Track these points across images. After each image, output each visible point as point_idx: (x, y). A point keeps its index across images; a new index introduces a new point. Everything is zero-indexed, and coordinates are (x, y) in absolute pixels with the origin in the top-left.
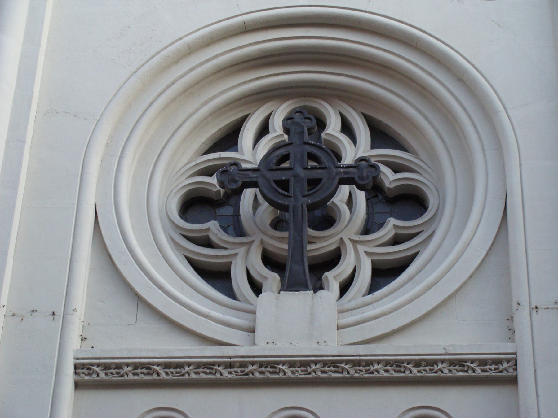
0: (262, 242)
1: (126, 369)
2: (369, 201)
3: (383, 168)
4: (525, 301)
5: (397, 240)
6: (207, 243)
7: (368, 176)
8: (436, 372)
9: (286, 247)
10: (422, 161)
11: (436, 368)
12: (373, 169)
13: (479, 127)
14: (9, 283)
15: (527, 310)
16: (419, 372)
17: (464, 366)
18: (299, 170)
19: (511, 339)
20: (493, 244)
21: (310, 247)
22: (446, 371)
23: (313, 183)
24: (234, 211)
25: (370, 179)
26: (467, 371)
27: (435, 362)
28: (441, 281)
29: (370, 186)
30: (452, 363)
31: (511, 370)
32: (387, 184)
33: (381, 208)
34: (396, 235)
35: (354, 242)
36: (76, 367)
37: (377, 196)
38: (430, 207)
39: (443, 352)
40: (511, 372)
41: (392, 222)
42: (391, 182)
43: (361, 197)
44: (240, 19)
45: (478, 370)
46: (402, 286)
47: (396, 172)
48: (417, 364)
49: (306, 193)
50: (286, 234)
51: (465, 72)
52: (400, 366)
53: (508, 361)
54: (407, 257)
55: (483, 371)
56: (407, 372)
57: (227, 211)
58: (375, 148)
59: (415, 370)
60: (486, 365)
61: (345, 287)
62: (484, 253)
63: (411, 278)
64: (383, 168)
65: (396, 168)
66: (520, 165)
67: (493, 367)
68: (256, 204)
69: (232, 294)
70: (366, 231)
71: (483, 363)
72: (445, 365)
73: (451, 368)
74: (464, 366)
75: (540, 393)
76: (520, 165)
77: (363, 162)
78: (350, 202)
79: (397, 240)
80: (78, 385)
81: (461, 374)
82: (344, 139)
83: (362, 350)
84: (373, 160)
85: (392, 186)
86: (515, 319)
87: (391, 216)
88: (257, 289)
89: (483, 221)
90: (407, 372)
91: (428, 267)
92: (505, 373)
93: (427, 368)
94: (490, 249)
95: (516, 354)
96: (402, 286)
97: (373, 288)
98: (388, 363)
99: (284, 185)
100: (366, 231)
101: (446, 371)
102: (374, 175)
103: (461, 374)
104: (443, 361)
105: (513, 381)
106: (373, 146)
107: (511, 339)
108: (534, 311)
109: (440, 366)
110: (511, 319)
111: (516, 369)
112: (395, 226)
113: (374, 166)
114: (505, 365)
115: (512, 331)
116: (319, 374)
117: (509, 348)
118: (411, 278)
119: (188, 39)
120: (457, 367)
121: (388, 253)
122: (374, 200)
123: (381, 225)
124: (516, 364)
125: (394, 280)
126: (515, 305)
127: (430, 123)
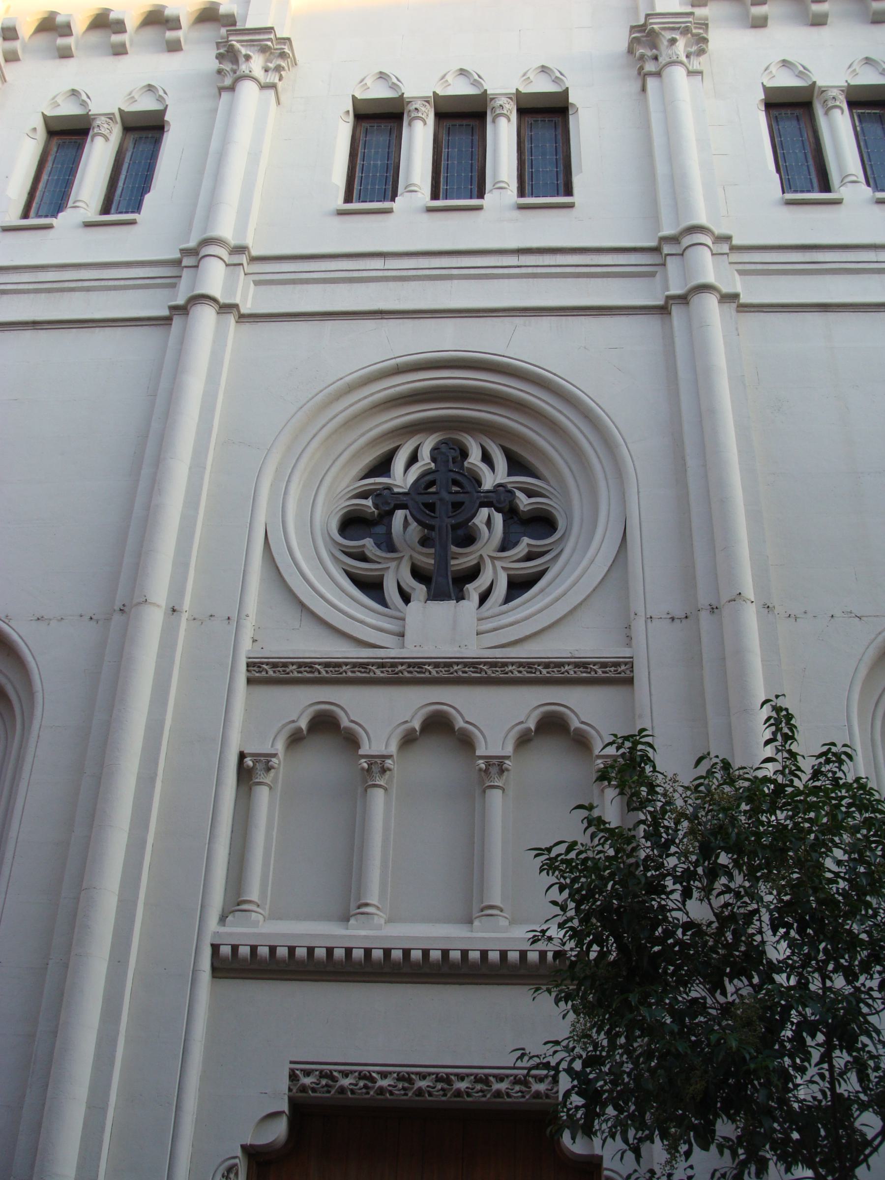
0: (411, 557)
1: (291, 668)
3: (519, 494)
4: (641, 612)
5: (529, 557)
6: (362, 557)
8: (563, 673)
9: (432, 562)
10: (550, 486)
11: (563, 670)
12: (510, 494)
15: (644, 619)
16: (548, 673)
17: (587, 668)
18: (444, 495)
19: (629, 645)
20: (614, 561)
21: (453, 562)
22: (572, 672)
23: (457, 506)
26: (590, 673)
27: (562, 665)
30: (577, 665)
31: (628, 672)
32: (522, 508)
34: (529, 553)
35: (492, 558)
36: (248, 665)
37: (512, 518)
38: (559, 528)
39: (569, 655)
41: (526, 540)
43: (498, 518)
44: (393, 362)
47: (529, 497)
48: (547, 666)
49: (451, 514)
50: (432, 551)
51: (591, 410)
53: (626, 664)
55: (604, 672)
56: (538, 673)
57: (380, 529)
59: (544, 671)
61: (484, 597)
62: (606, 569)
63: (542, 591)
64: (519, 494)
65: (530, 494)
66: (638, 492)
67: (612, 669)
68: (406, 524)
69: (383, 602)
70: (503, 548)
71: (604, 665)
72: (570, 667)
73: (576, 669)
74: (587, 668)
77: (501, 488)
78: (489, 523)
79: (529, 557)
80: (250, 681)
81: (584, 675)
82: (484, 467)
83: (498, 653)
84: (509, 486)
86: (632, 627)
87: (525, 536)
88: (406, 598)
90: (538, 673)
92: (623, 675)
93: (555, 670)
95: (632, 658)
97: (508, 599)
98: (521, 665)
99: (431, 507)
100: (503, 548)
101: (572, 672)
103: (584, 675)
104: (569, 664)
106: (510, 474)
107: (629, 645)
108: (649, 620)
109: (567, 668)
111: (632, 671)
112: (528, 545)
113: (511, 492)
114: (623, 667)
115: (629, 637)
116: (460, 673)
117: (626, 652)
118: (542, 591)
119: (348, 379)
125: (526, 592)
126: (632, 615)
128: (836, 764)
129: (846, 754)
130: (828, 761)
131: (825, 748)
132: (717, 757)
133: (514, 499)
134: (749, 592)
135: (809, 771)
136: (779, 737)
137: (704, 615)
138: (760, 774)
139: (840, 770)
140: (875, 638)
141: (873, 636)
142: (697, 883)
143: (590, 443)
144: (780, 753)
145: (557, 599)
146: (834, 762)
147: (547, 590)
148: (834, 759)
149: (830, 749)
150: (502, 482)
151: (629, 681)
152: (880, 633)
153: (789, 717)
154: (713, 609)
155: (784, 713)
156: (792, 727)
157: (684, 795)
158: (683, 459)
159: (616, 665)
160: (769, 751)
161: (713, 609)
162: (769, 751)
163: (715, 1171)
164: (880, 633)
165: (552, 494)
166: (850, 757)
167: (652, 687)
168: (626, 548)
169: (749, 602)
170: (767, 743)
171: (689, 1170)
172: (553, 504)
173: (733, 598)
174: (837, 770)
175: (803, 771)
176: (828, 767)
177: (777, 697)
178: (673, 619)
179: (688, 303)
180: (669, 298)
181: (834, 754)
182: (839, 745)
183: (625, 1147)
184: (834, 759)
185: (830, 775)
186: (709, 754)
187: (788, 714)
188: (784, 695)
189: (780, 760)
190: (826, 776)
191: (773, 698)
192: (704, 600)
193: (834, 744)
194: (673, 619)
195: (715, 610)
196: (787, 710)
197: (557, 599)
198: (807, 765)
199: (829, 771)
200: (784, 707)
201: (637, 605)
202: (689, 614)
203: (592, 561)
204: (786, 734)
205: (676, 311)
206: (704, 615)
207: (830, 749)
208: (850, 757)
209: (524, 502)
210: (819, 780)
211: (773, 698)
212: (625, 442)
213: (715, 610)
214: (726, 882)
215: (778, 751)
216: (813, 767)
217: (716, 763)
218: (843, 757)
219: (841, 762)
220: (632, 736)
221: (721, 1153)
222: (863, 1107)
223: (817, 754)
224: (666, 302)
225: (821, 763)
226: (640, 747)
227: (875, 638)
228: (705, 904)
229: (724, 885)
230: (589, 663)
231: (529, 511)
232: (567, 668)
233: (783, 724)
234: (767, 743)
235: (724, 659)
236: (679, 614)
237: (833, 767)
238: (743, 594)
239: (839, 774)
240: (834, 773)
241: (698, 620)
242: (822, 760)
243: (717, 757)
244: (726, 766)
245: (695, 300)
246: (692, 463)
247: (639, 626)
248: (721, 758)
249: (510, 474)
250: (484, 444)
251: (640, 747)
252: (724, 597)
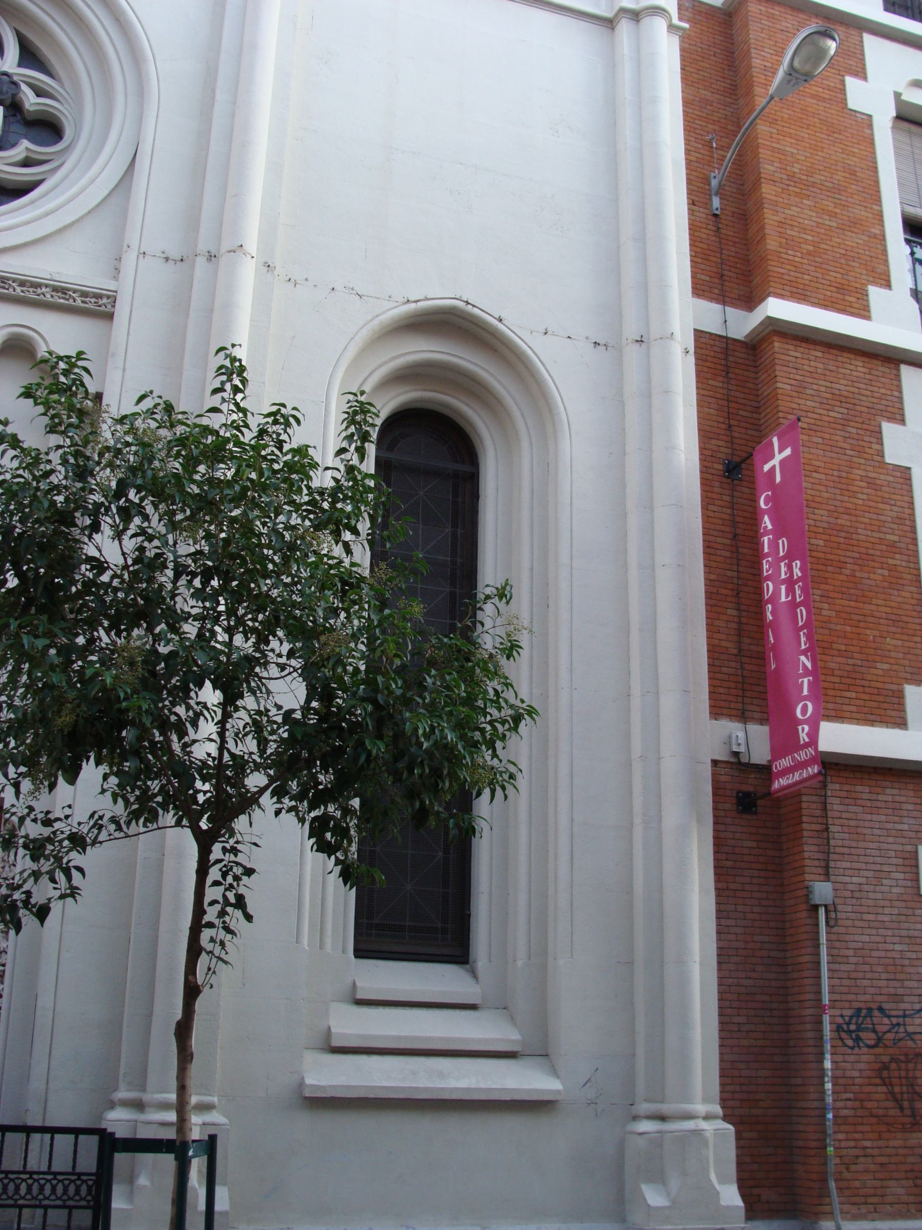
2: (725, 340)
3: (24, 87)
4: (135, 244)
5: (27, 163)
7: (7, 92)
8: (38, 295)
10: (64, 89)
11: (39, 291)
12: (13, 86)
13: (126, 72)
14: (256, 240)
15: (136, 253)
16: (22, 291)
17: (66, 294)
19: (116, 278)
20: (116, 186)
22: (48, 296)
24: (735, 340)
25: (10, 95)
26: (68, 300)
27: (39, 285)
28: (61, 210)
29: (8, 102)
30: (55, 289)
31: (109, 306)
32: (27, 106)
33: (17, 128)
34: (27, 158)
37: (15, 115)
38: (65, 137)
39: (49, 277)
40: (109, 308)
41: (25, 144)
42: (31, 104)
45: (79, 300)
46: (25, 206)
47: (38, 96)
48: (22, 284)
51: (123, 12)
52: (5, 283)
53: (108, 297)
54: (31, 181)
55: (83, 302)
56: (11, 290)
58: (695, 335)
59: (18, 289)
60: (87, 297)
62: (106, 192)
63: (32, 202)
64: (24, 87)
65: (39, 93)
66: (157, 116)
67: (93, 300)
71: (84, 294)
72: (48, 290)
73: (54, 293)
74: (66, 294)
75: (131, 332)
76: (157, 116)
77: (5, 77)
79: (27, 163)
81: (62, 301)
84: (15, 78)
85: (32, 109)
86: (123, 260)
87: (26, 138)
89: (111, 161)
90: (11, 290)
91: (50, 195)
92: (103, 308)
93: (31, 290)
94: (113, 190)
95: (116, 292)
96: (25, 206)
101: (48, 296)
102: (14, 92)
103: (62, 301)
104: (47, 286)
105: (110, 316)
106: (20, 65)
107: (116, 278)
108: (142, 256)
109: (44, 290)
110: (119, 259)
111: (114, 306)
112: (27, 149)
113: (15, 84)
114: (105, 301)
115: (117, 270)
117: (111, 285)
118: (32, 202)
120: (60, 294)
121: (16, 174)
122: (12, 119)
123: (14, 145)
124: (115, 302)
125: (12, 201)
126: (125, 247)
127: (80, 55)
128: (283, 427)
129: (294, 417)
130: (276, 422)
131: (275, 409)
132: (160, 397)
133: (18, 93)
134: (252, 245)
135: (255, 429)
136: (228, 387)
137: (201, 261)
138: (205, 421)
139: (285, 432)
140: (372, 320)
141: (370, 317)
142: (108, 520)
143: (116, 51)
144: (226, 404)
145: (47, 214)
146: (281, 424)
147: (38, 203)
148: (282, 420)
149: (279, 410)
150: (10, 71)
151: (109, 317)
152: (377, 316)
153: (242, 369)
154: (211, 257)
155: (237, 364)
156: (244, 381)
157: (113, 429)
158: (213, 91)
159: (98, 296)
160: (216, 401)
161: (211, 257)
162: (216, 401)
163: (95, 812)
164: (377, 316)
165: (65, 99)
166: (298, 422)
167: (132, 327)
168: (132, 175)
169: (249, 257)
170: (216, 391)
171: (67, 808)
172: (63, 110)
173: (233, 249)
174: (282, 432)
175: (250, 429)
176: (275, 428)
177: (233, 346)
178: (167, 259)
179: (638, 21)
180: (623, 10)
181: (283, 416)
182: (289, 407)
183: (5, 781)
184: (282, 420)
185: (274, 436)
186: (151, 392)
187: (241, 365)
188: (240, 345)
189: (225, 411)
190: (271, 436)
191: (230, 347)
192: (203, 246)
193: (284, 406)
194: (167, 259)
195: (213, 259)
196: (240, 361)
197: (47, 214)
198: (254, 422)
199: (274, 432)
200: (238, 357)
201: (132, 236)
202: (185, 257)
203: (93, 181)
204: (236, 386)
205: (625, 27)
206: (201, 261)
207: (279, 410)
208: (298, 422)
209: (30, 101)
210: (263, 439)
211: (230, 347)
212: (154, 57)
213: (213, 259)
214: (140, 523)
215: (224, 400)
216: (259, 425)
217: (159, 404)
218: (291, 420)
219: (287, 424)
220: (68, 357)
221: (115, 802)
222: (257, 767)
223: (265, 413)
224: (616, 15)
225: (268, 423)
226: (76, 370)
227: (372, 320)
228: (116, 542)
229: (139, 527)
230: (69, 289)
231: (35, 111)
232: (44, 290)
233: (235, 376)
234: (216, 391)
235: (211, 311)
236: (175, 254)
237: (279, 428)
238: (245, 247)
239: (284, 437)
240: (279, 435)
241: (194, 262)
242: (270, 420)
243: (160, 397)
244: (169, 408)
245: (646, 22)
246: (221, 96)
247: (130, 260)
248: (164, 399)
249: (20, 65)
250: (18, 28)
251: (76, 370)
252: (226, 246)
